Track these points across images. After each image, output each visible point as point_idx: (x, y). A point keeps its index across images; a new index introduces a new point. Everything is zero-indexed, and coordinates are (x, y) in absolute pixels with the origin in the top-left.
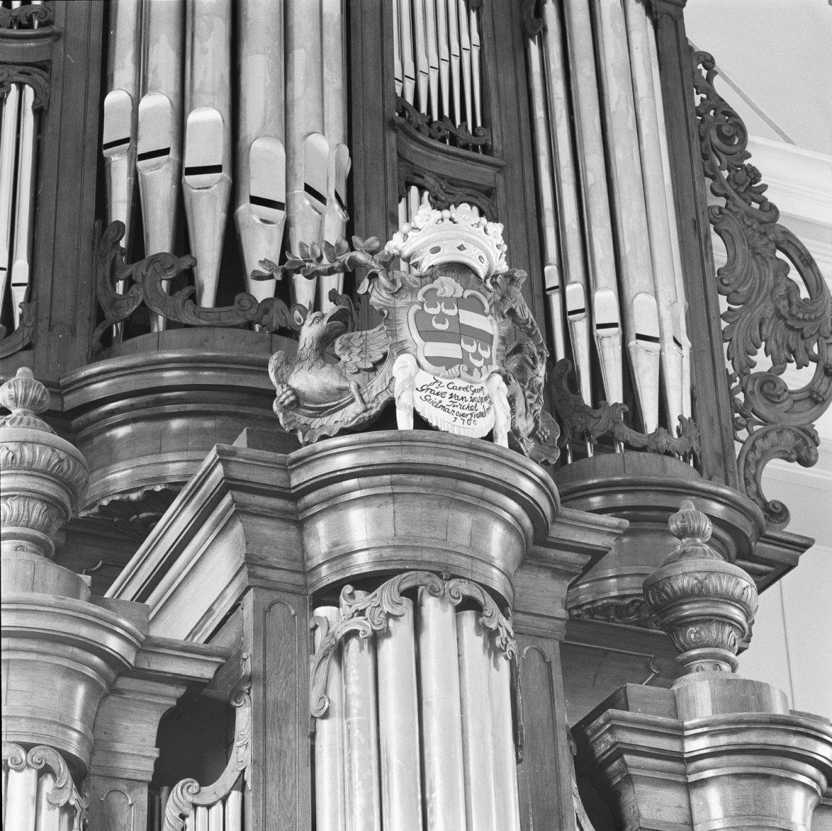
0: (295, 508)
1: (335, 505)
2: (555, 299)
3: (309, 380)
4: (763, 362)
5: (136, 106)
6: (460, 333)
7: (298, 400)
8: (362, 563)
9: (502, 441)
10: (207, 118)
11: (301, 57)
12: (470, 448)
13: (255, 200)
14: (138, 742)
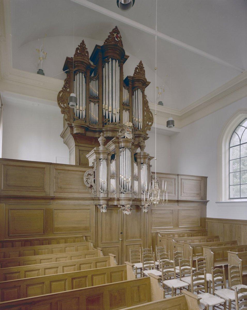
0: (119, 143)
1: (121, 143)
2: (133, 119)
3: (120, 134)
4: (148, 122)
5: (105, 106)
6: (129, 131)
7: (119, 135)
8: (123, 146)
9: (131, 139)
10: (110, 107)
11: (117, 101)
12: (129, 139)
13: (114, 114)
14: (110, 157)
